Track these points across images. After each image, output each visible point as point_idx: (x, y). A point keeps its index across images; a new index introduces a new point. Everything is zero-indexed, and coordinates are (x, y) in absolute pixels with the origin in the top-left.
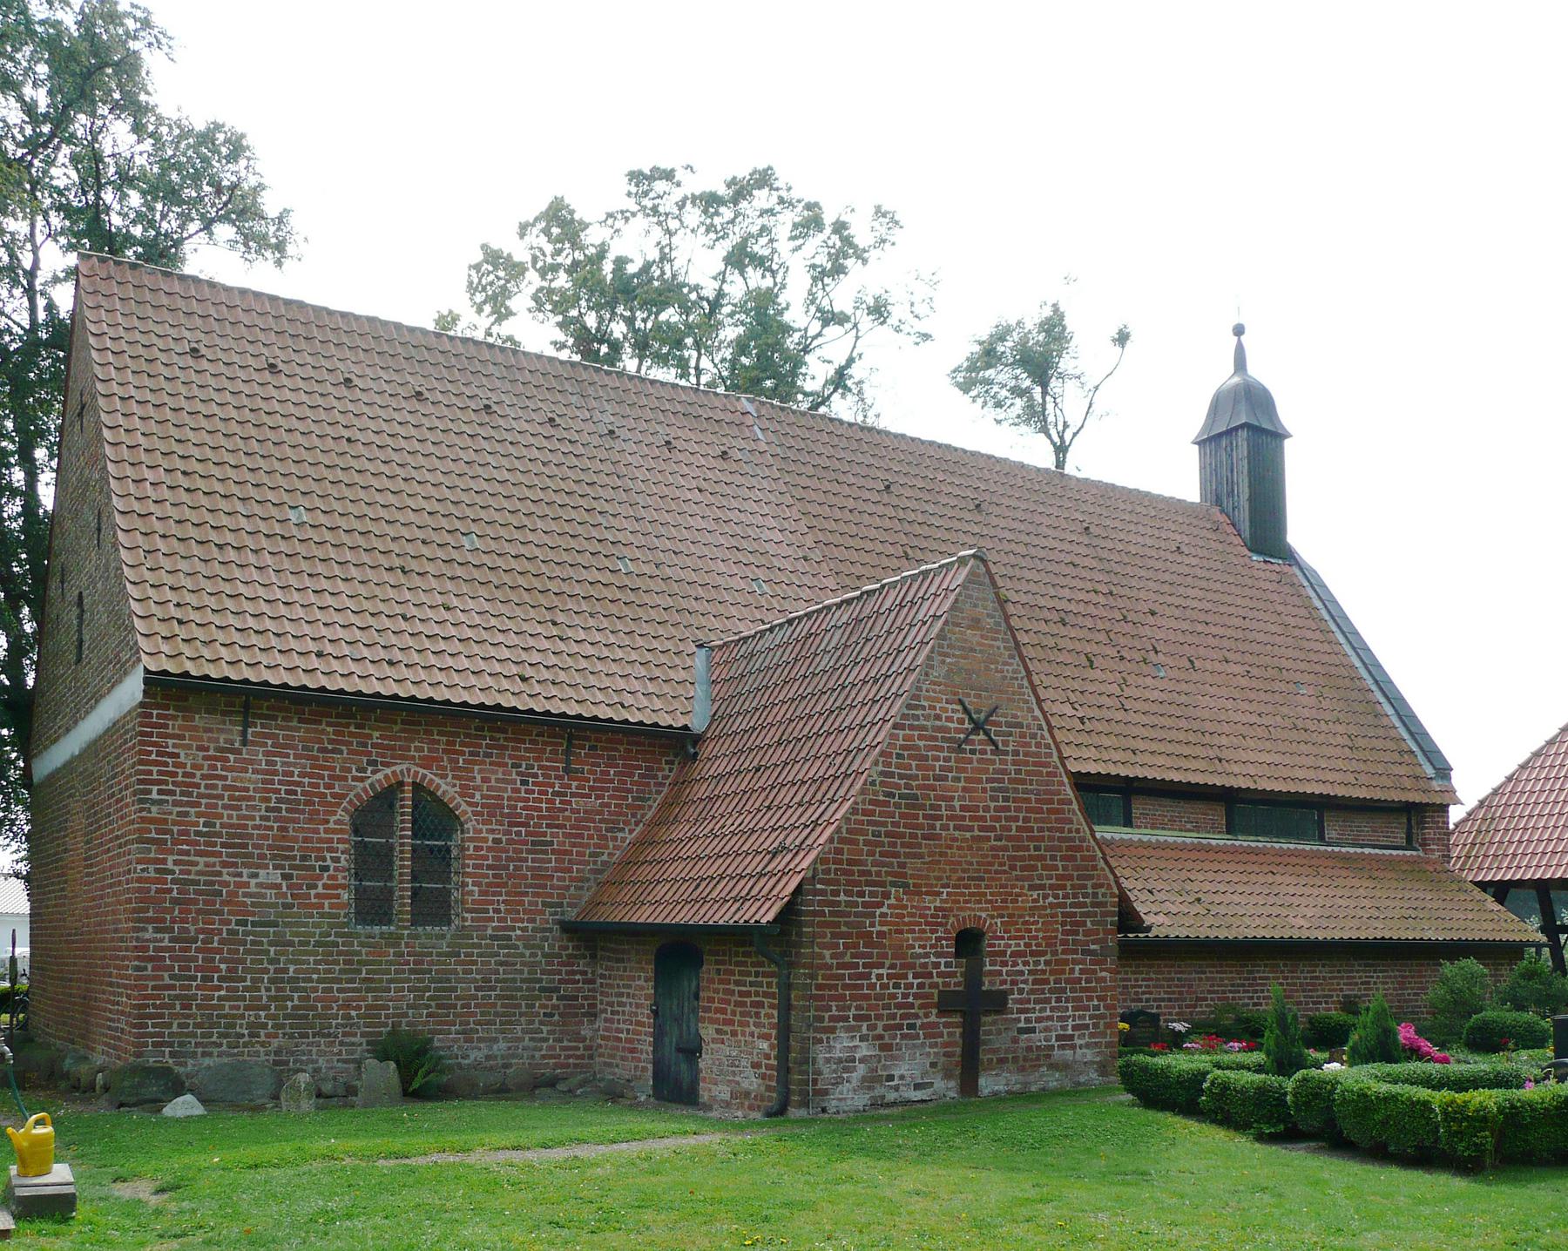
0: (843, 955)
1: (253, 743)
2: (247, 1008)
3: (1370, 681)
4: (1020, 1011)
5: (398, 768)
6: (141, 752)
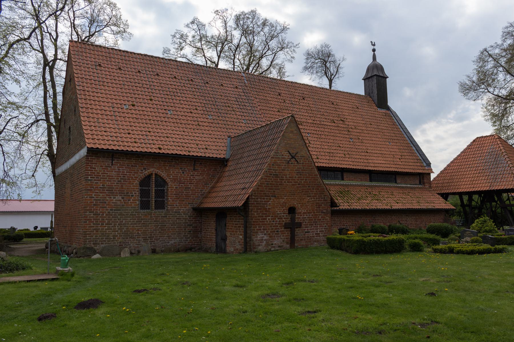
0: (259, 214)
1: (115, 165)
2: (112, 231)
3: (409, 141)
4: (305, 227)
5: (151, 170)
6: (86, 168)
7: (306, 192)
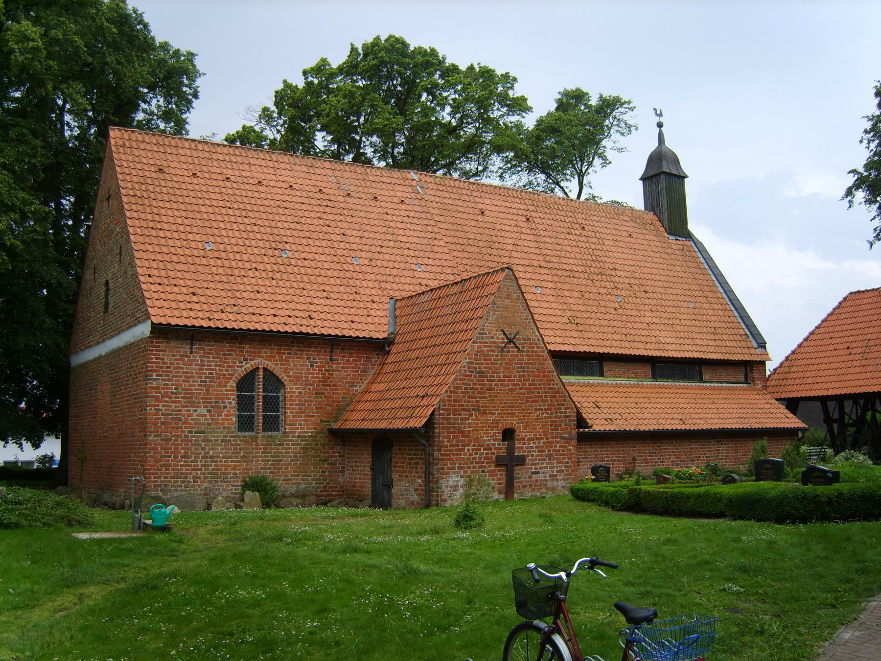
3: (727, 300)
7: (534, 401)
